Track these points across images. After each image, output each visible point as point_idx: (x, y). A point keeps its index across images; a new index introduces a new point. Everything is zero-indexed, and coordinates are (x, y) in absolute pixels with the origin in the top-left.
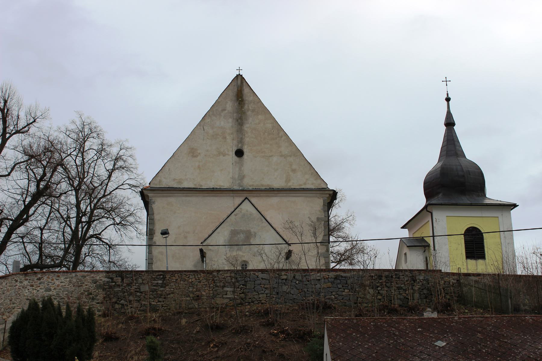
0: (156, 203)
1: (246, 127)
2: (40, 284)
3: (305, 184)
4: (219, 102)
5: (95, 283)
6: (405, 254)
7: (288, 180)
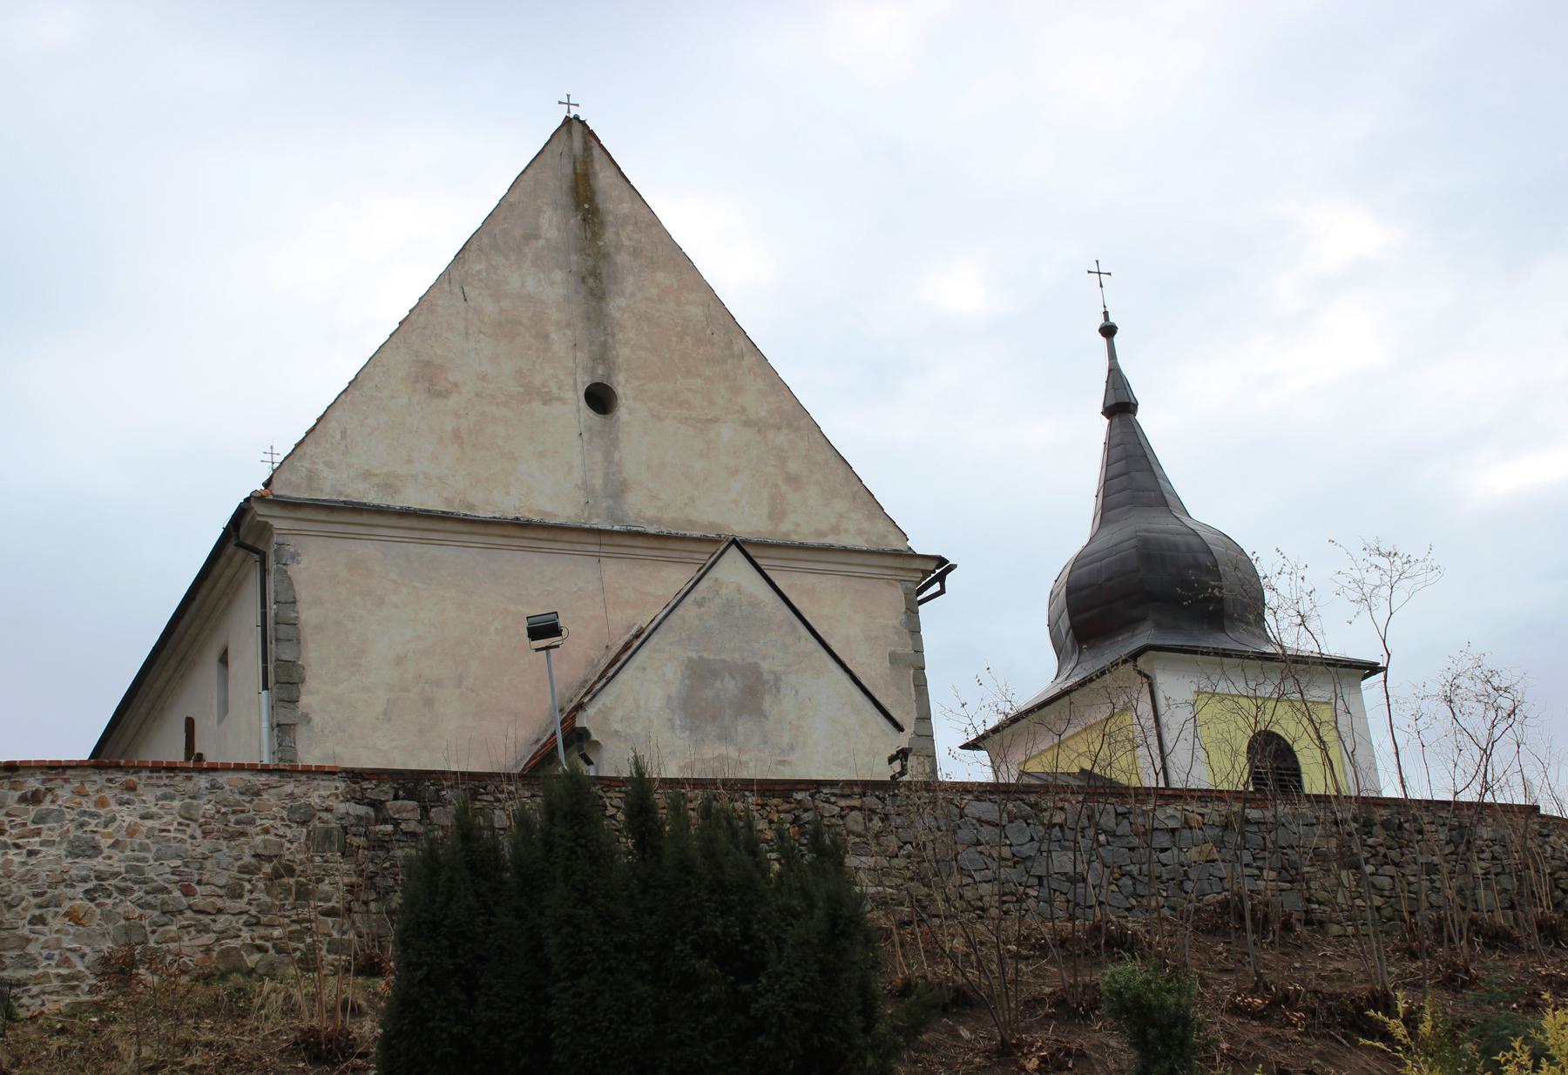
0: (304, 561)
1: (617, 306)
2: (40, 819)
3: (835, 530)
4: (511, 205)
5: (303, 823)
7: (777, 512)
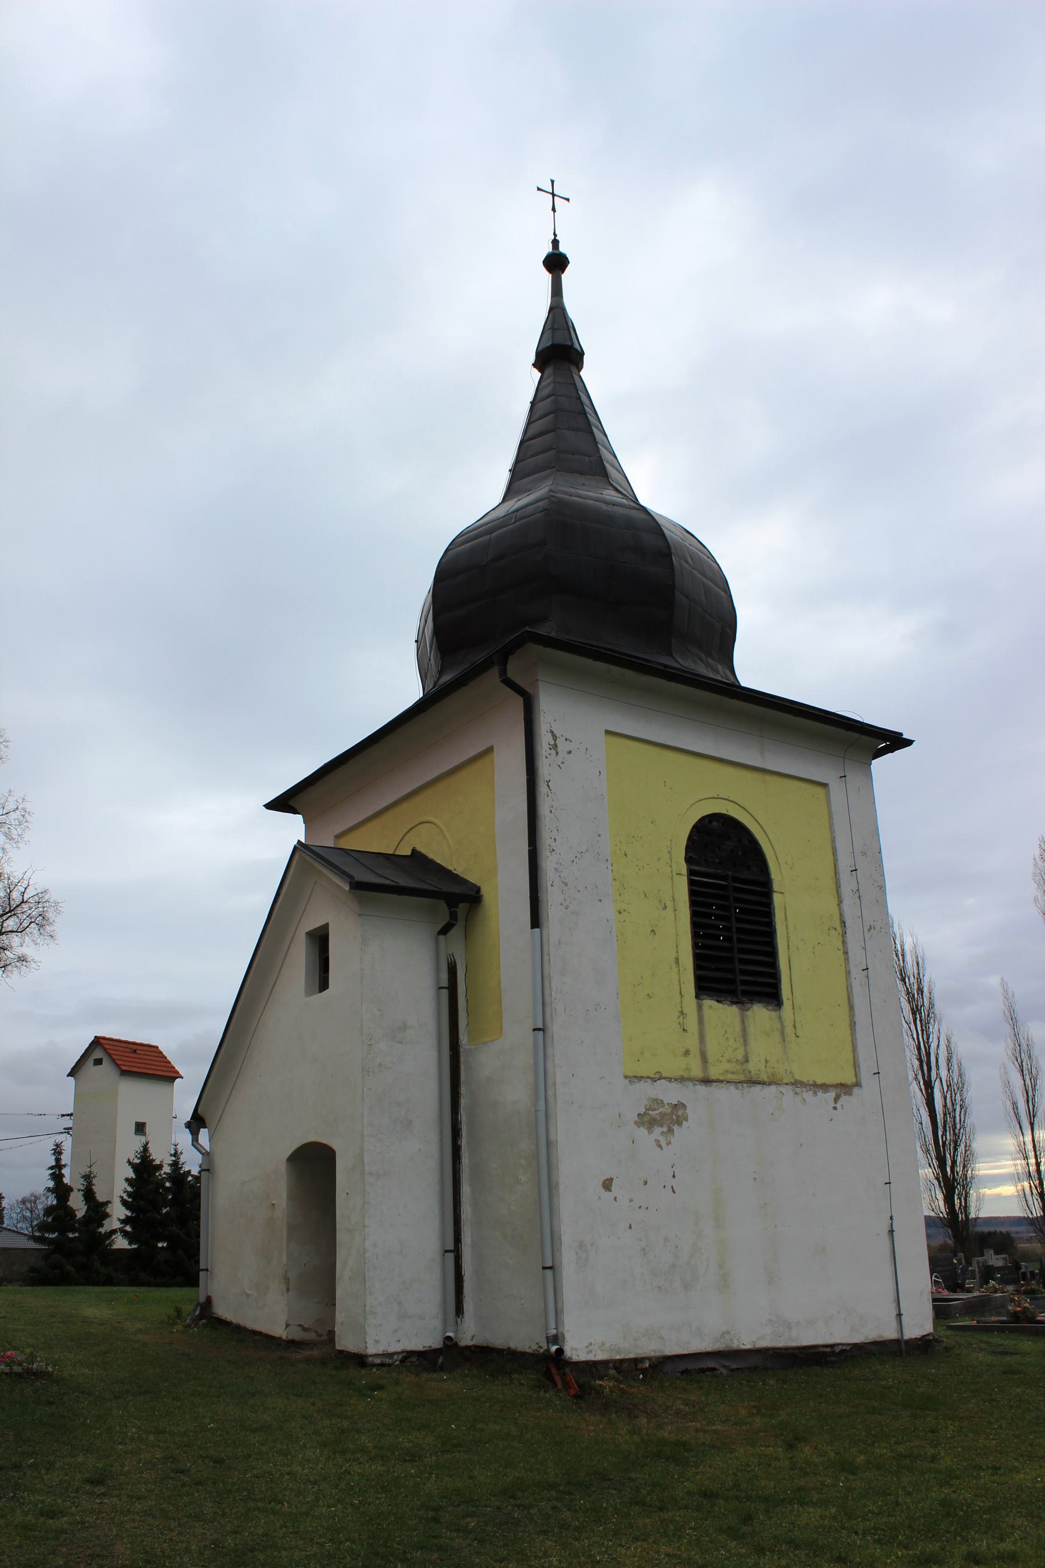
6: (320, 939)
